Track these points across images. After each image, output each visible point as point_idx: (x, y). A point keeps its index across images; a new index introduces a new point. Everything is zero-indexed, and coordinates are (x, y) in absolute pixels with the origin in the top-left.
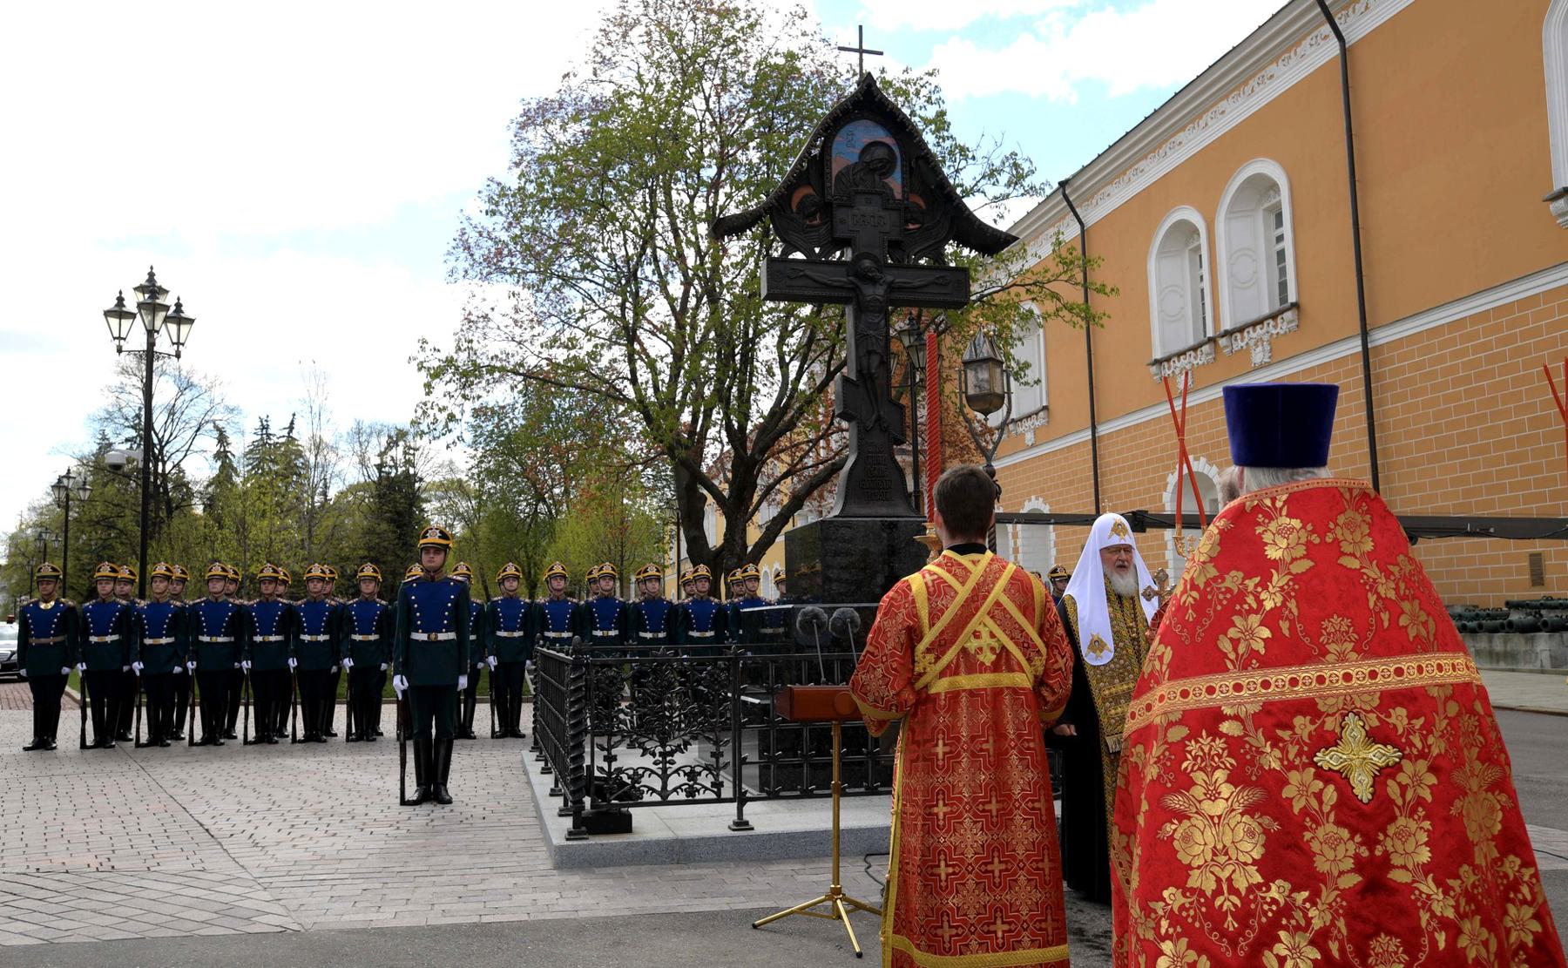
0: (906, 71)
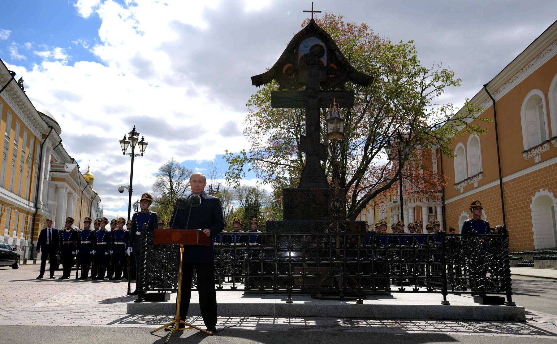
0: (401, 42)
